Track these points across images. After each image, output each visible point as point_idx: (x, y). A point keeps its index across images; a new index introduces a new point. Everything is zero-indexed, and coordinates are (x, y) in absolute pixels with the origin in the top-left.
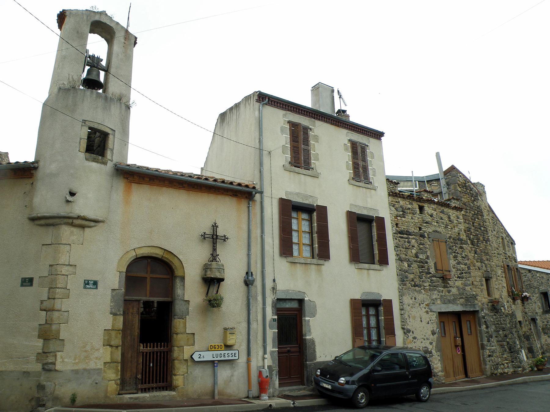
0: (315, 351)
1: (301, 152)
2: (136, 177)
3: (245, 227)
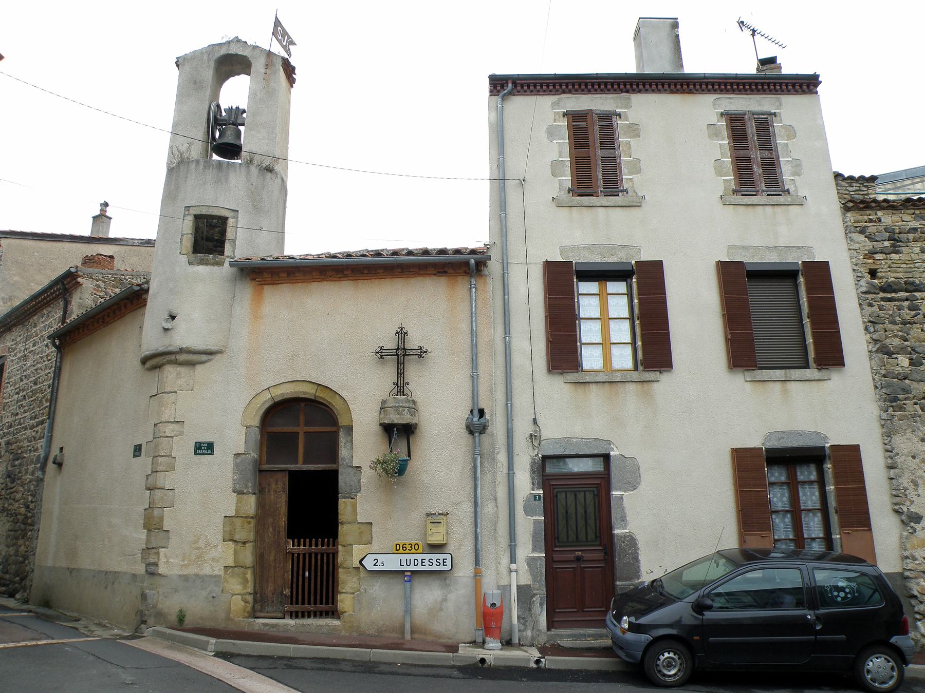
0: (637, 560)
1: (596, 165)
2: (266, 275)
3: (465, 327)
